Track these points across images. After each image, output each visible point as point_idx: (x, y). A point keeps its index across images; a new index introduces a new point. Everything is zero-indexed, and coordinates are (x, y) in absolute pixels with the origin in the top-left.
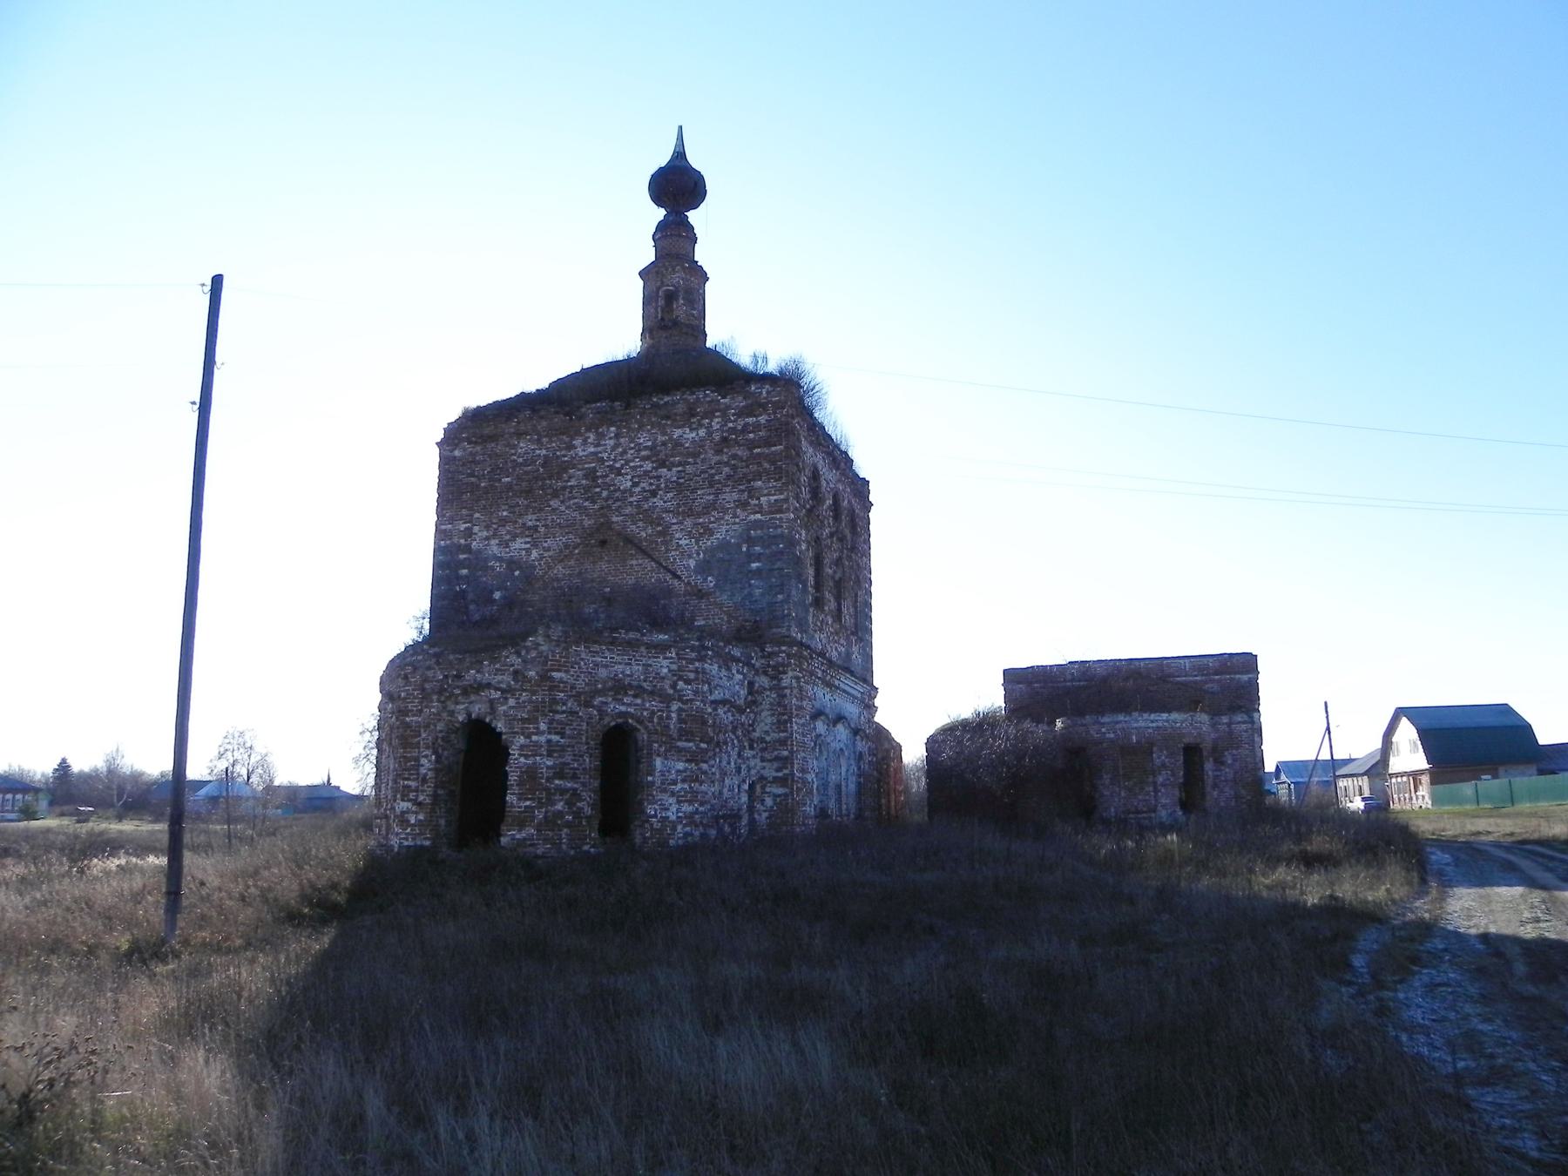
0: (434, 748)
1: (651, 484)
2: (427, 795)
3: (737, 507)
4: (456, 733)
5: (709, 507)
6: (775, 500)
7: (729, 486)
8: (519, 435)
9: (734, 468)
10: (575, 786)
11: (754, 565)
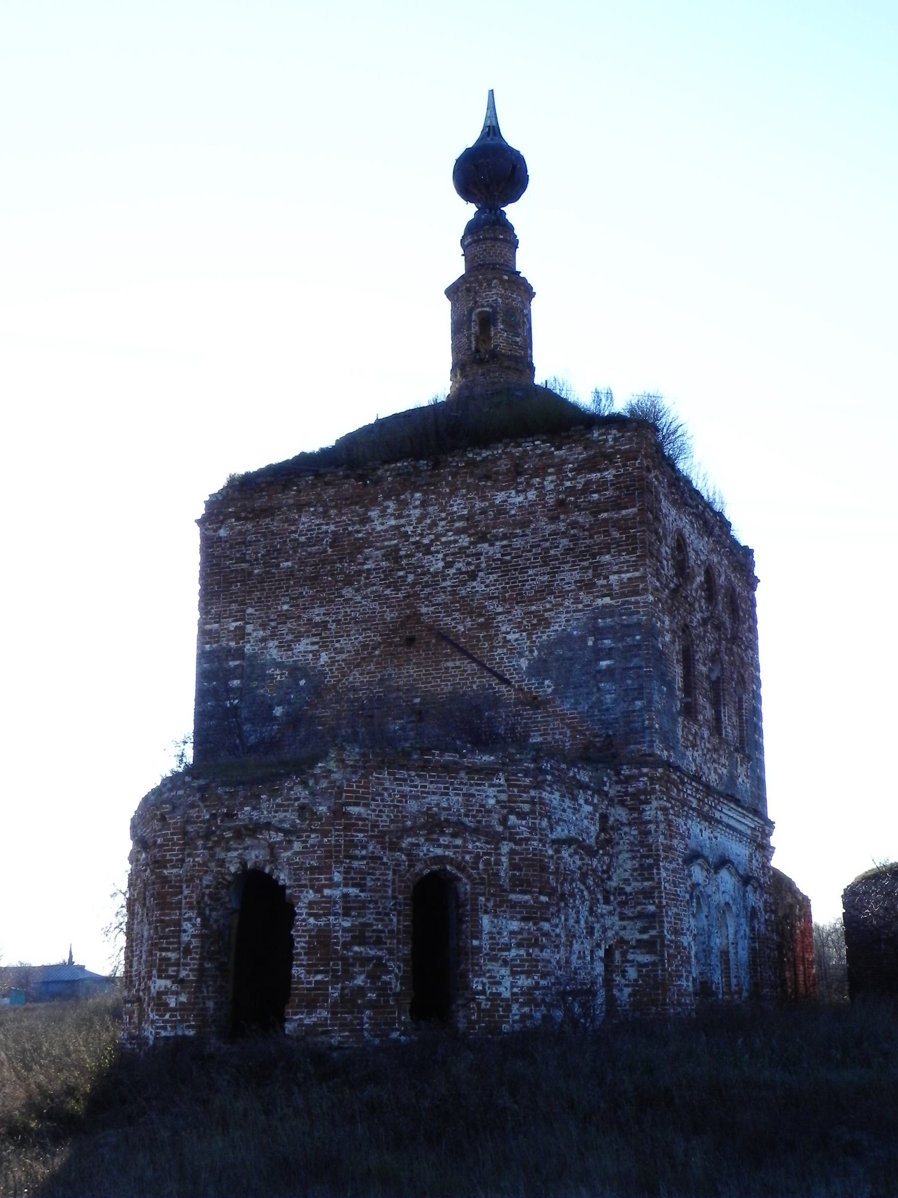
0: (199, 909)
1: (469, 564)
2: (191, 970)
3: (580, 588)
6: (628, 579)
7: (568, 562)
8: (300, 507)
10: (379, 953)
11: (604, 664)
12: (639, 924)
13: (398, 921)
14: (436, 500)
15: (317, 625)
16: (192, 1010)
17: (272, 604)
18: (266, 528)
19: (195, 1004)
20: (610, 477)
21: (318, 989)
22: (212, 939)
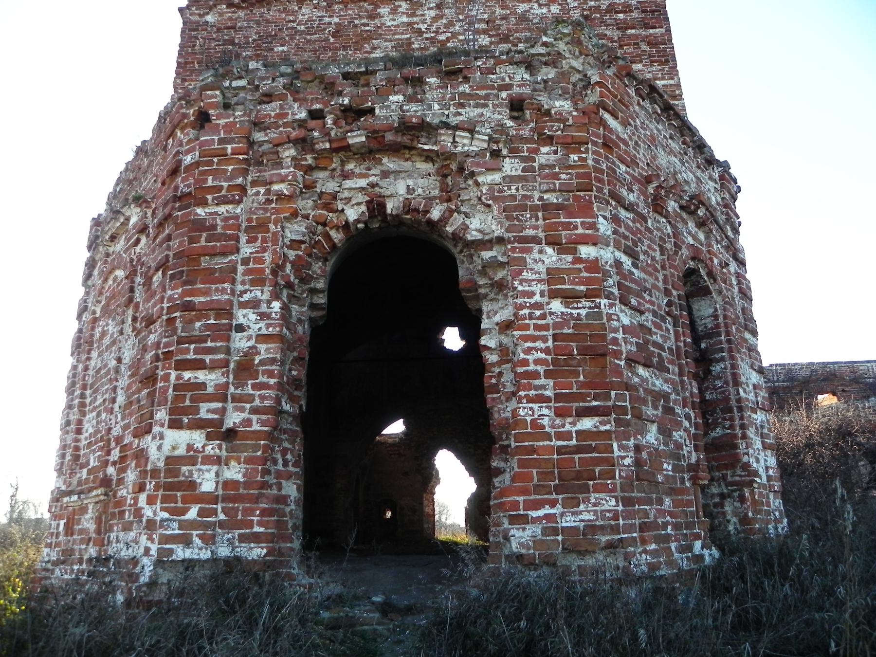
0: (276, 284)
2: (255, 411)
4: (326, 260)
13: (676, 333)
16: (256, 499)
19: (264, 485)
21: (591, 449)
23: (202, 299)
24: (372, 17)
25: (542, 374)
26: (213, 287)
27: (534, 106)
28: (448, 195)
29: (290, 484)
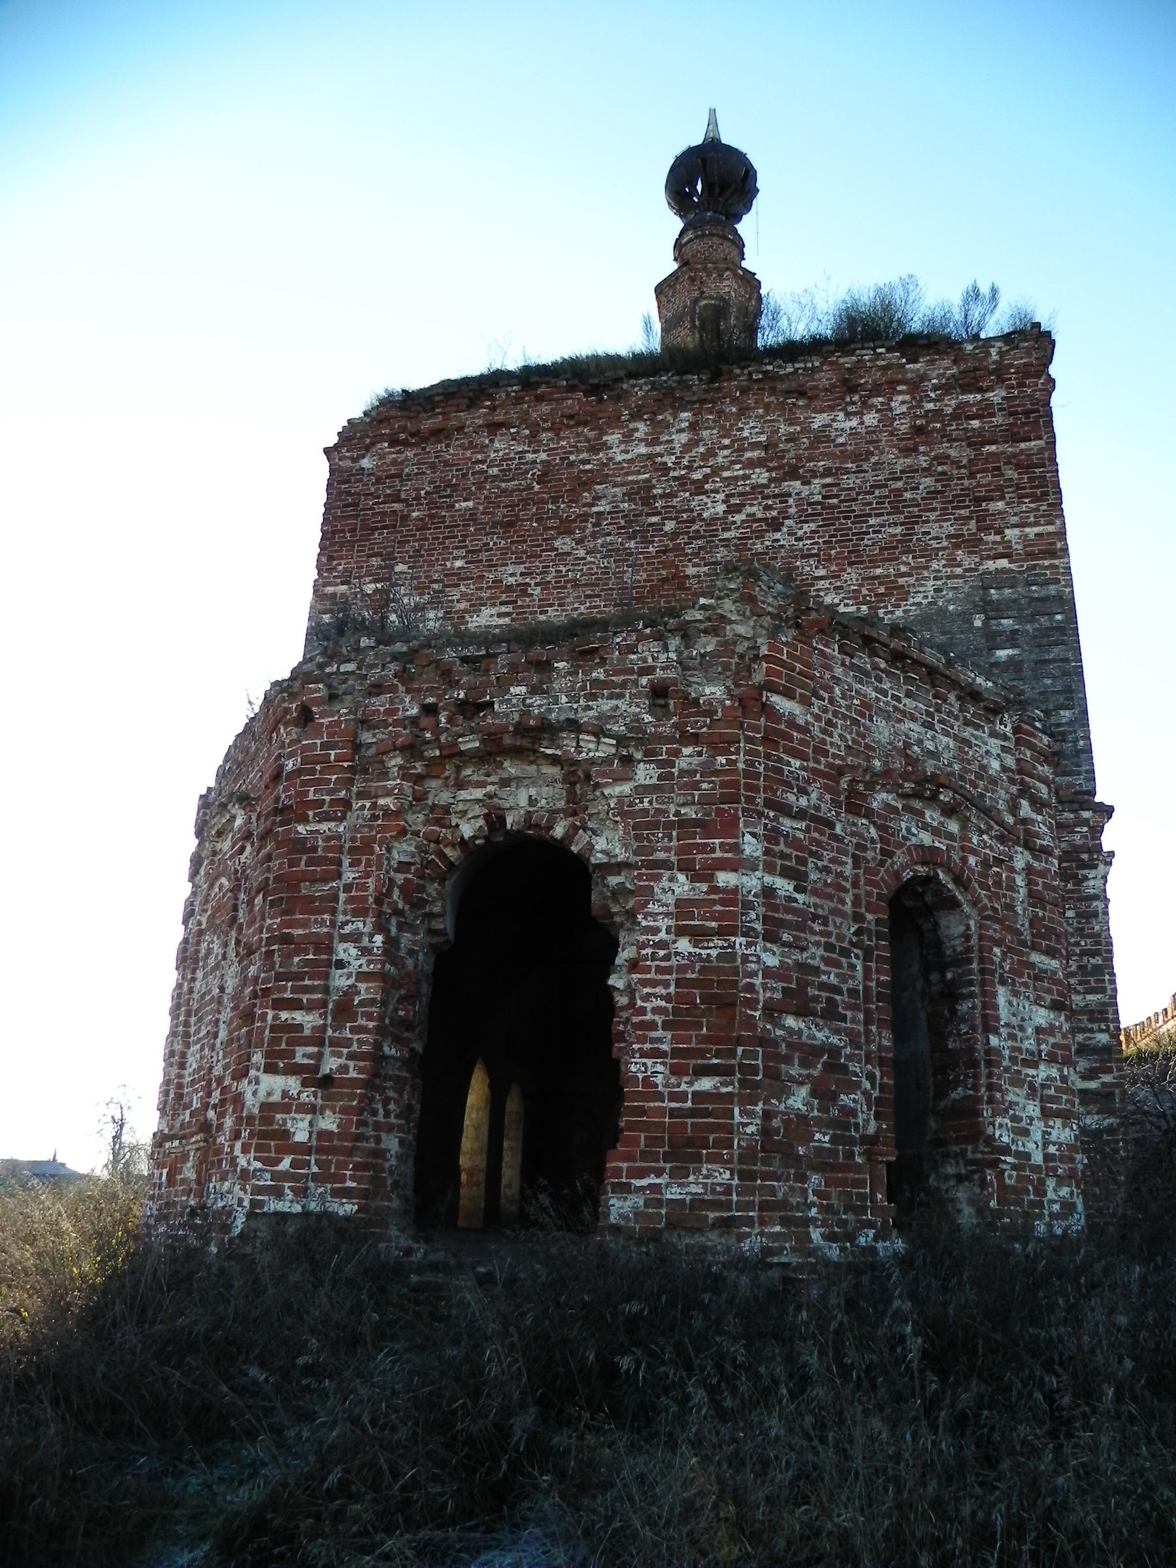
0: (379, 914)
1: (768, 508)
2: (352, 1056)
3: (957, 546)
4: (443, 880)
5: (896, 548)
6: (1036, 535)
7: (935, 509)
8: (494, 427)
9: (943, 477)
10: (834, 1040)
11: (1002, 654)
12: (1083, 1064)
13: (867, 971)
14: (714, 421)
15: (509, 588)
16: (350, 1152)
17: (437, 560)
18: (436, 457)
19: (359, 1137)
20: (997, 400)
21: (706, 1113)
22: (403, 992)
23: (300, 932)
24: (594, 450)
25: (660, 1024)
26: (313, 918)
27: (680, 695)
28: (575, 807)
29: (391, 1137)
